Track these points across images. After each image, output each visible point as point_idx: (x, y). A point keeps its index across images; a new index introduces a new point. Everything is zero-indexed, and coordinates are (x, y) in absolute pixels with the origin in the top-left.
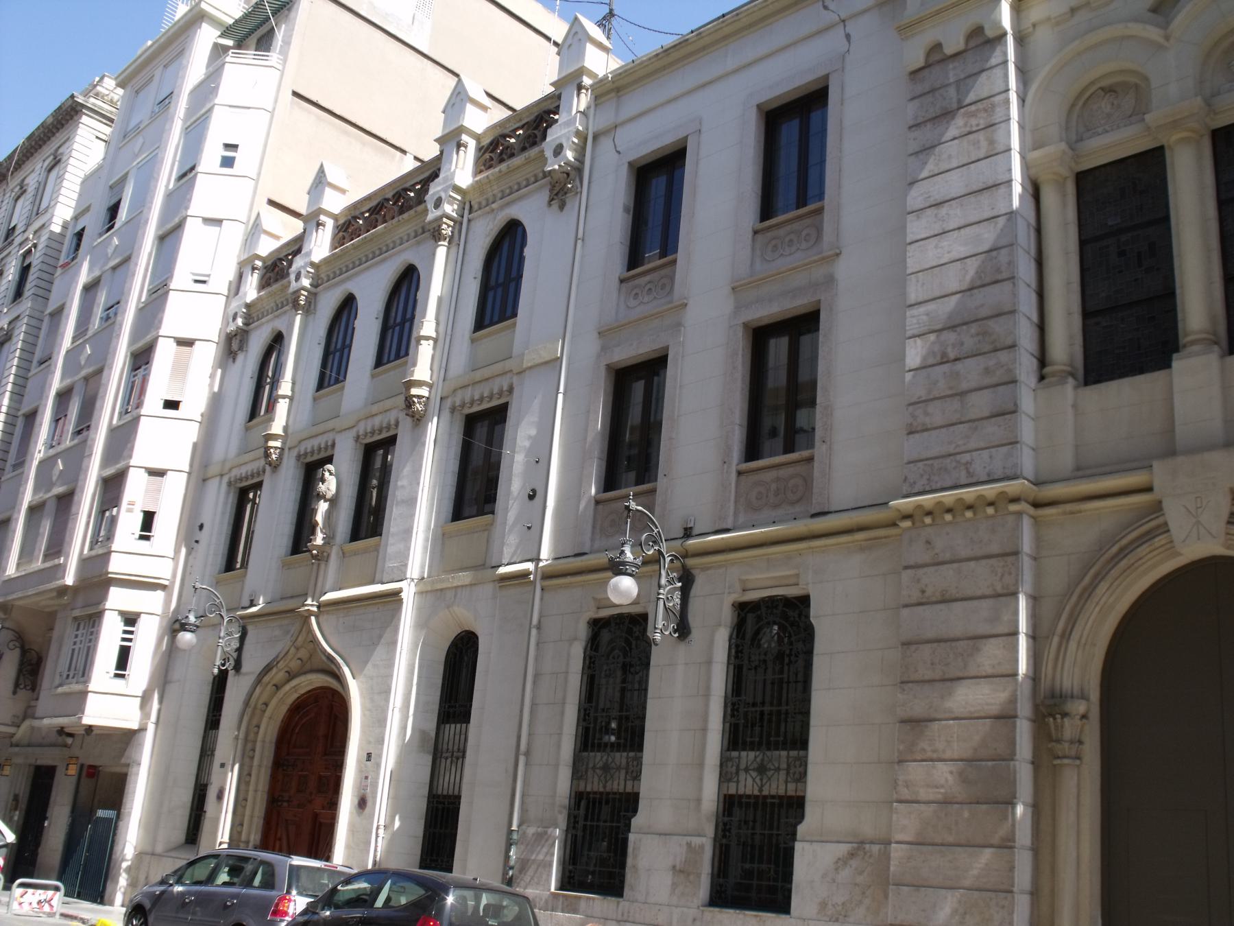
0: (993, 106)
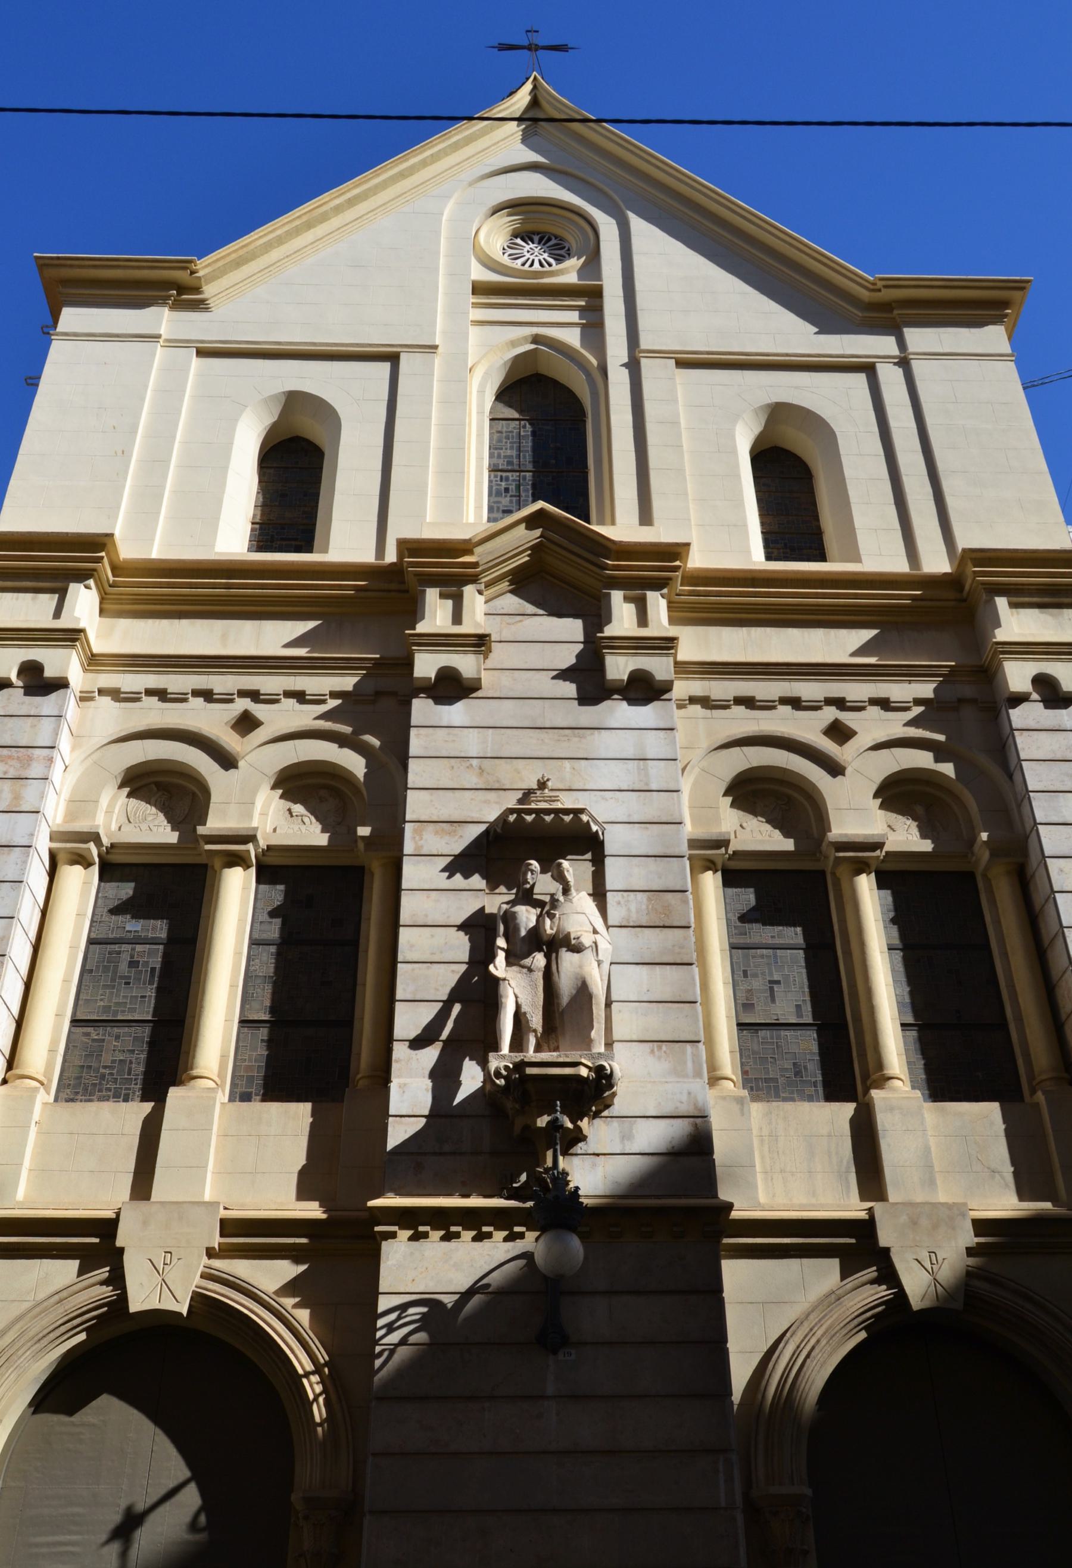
0: (30, 759)
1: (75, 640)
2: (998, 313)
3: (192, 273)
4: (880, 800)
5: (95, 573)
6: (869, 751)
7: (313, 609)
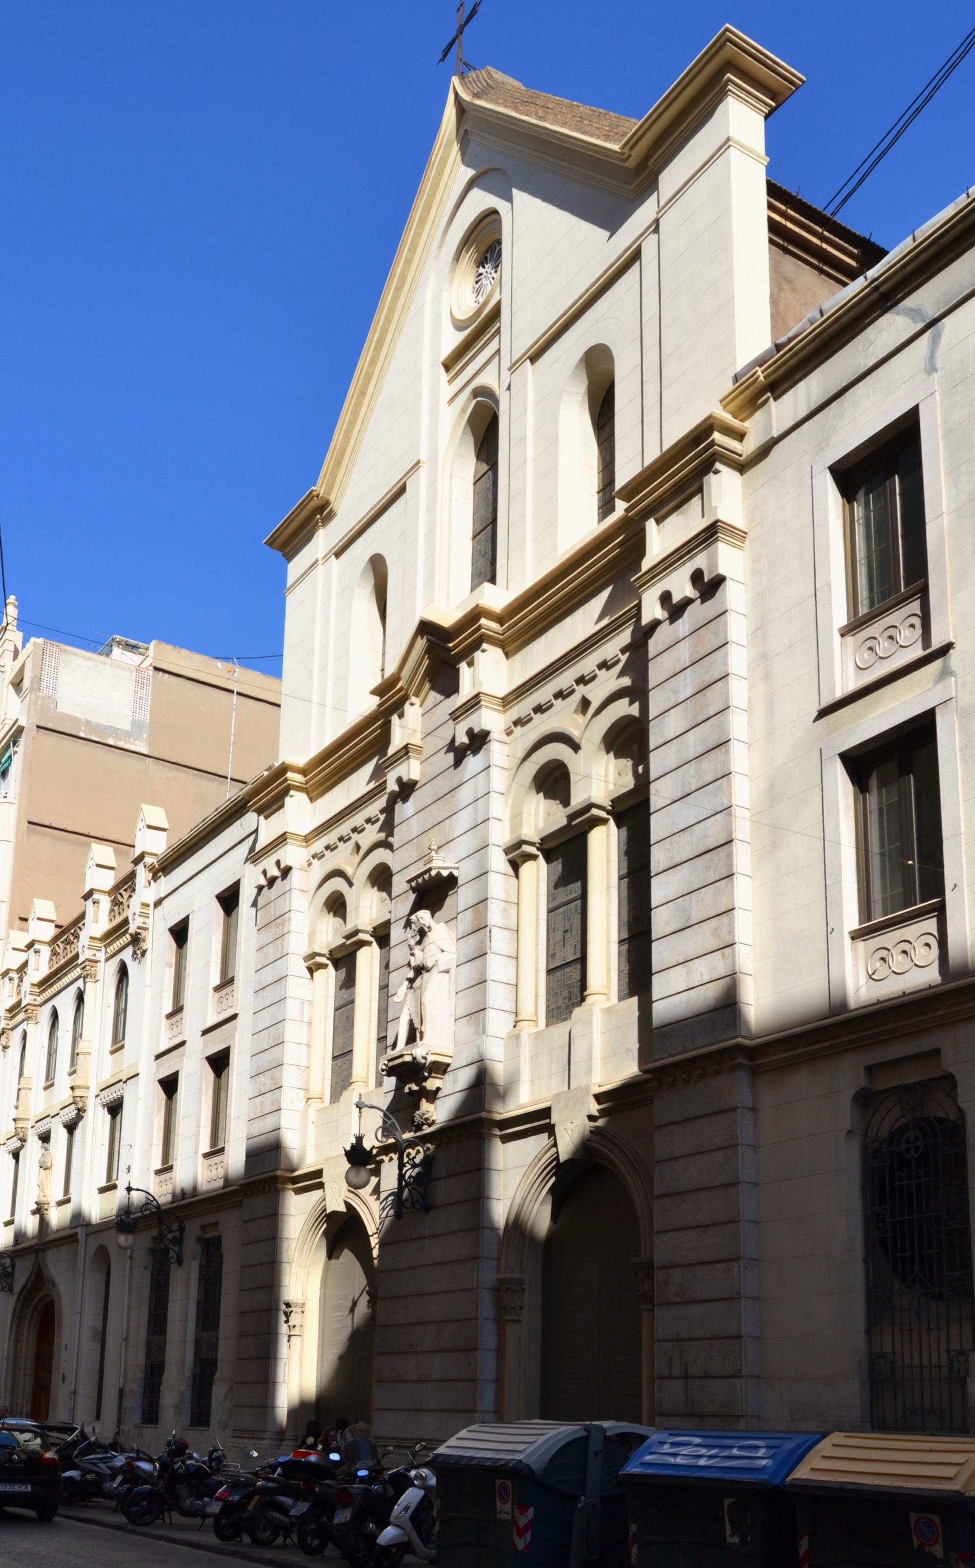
1: (286, 839)
2: (719, 87)
3: (318, 496)
4: (612, 753)
5: (483, 637)
6: (595, 718)
7: (368, 754)
